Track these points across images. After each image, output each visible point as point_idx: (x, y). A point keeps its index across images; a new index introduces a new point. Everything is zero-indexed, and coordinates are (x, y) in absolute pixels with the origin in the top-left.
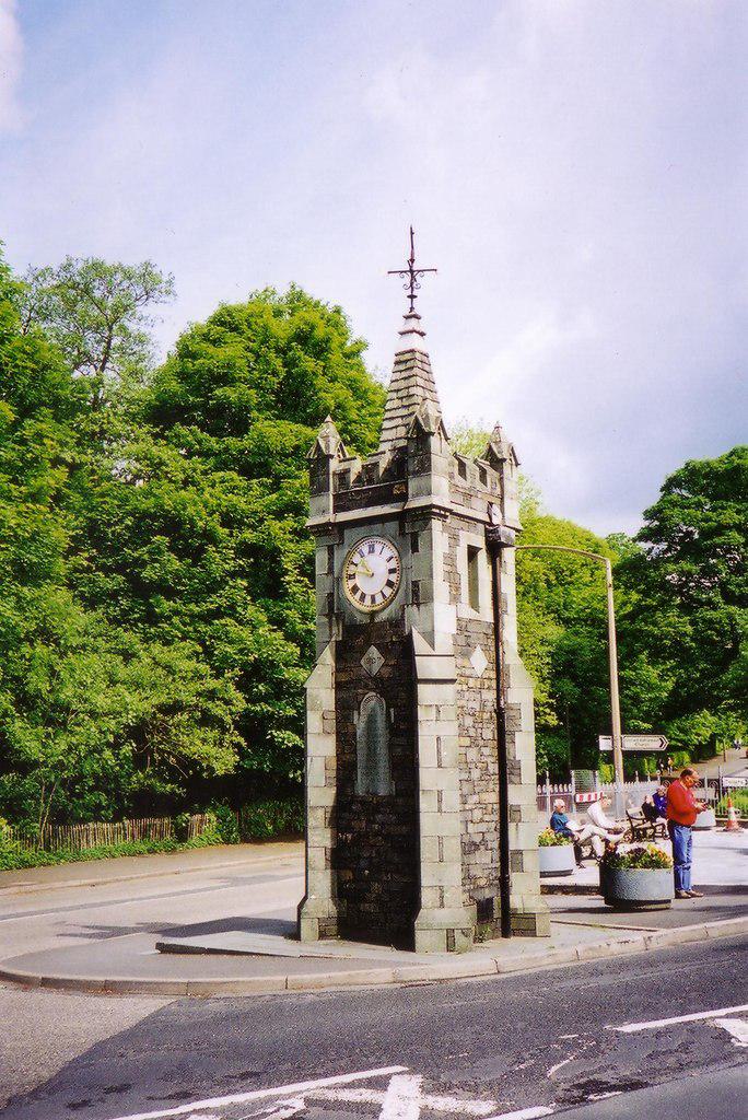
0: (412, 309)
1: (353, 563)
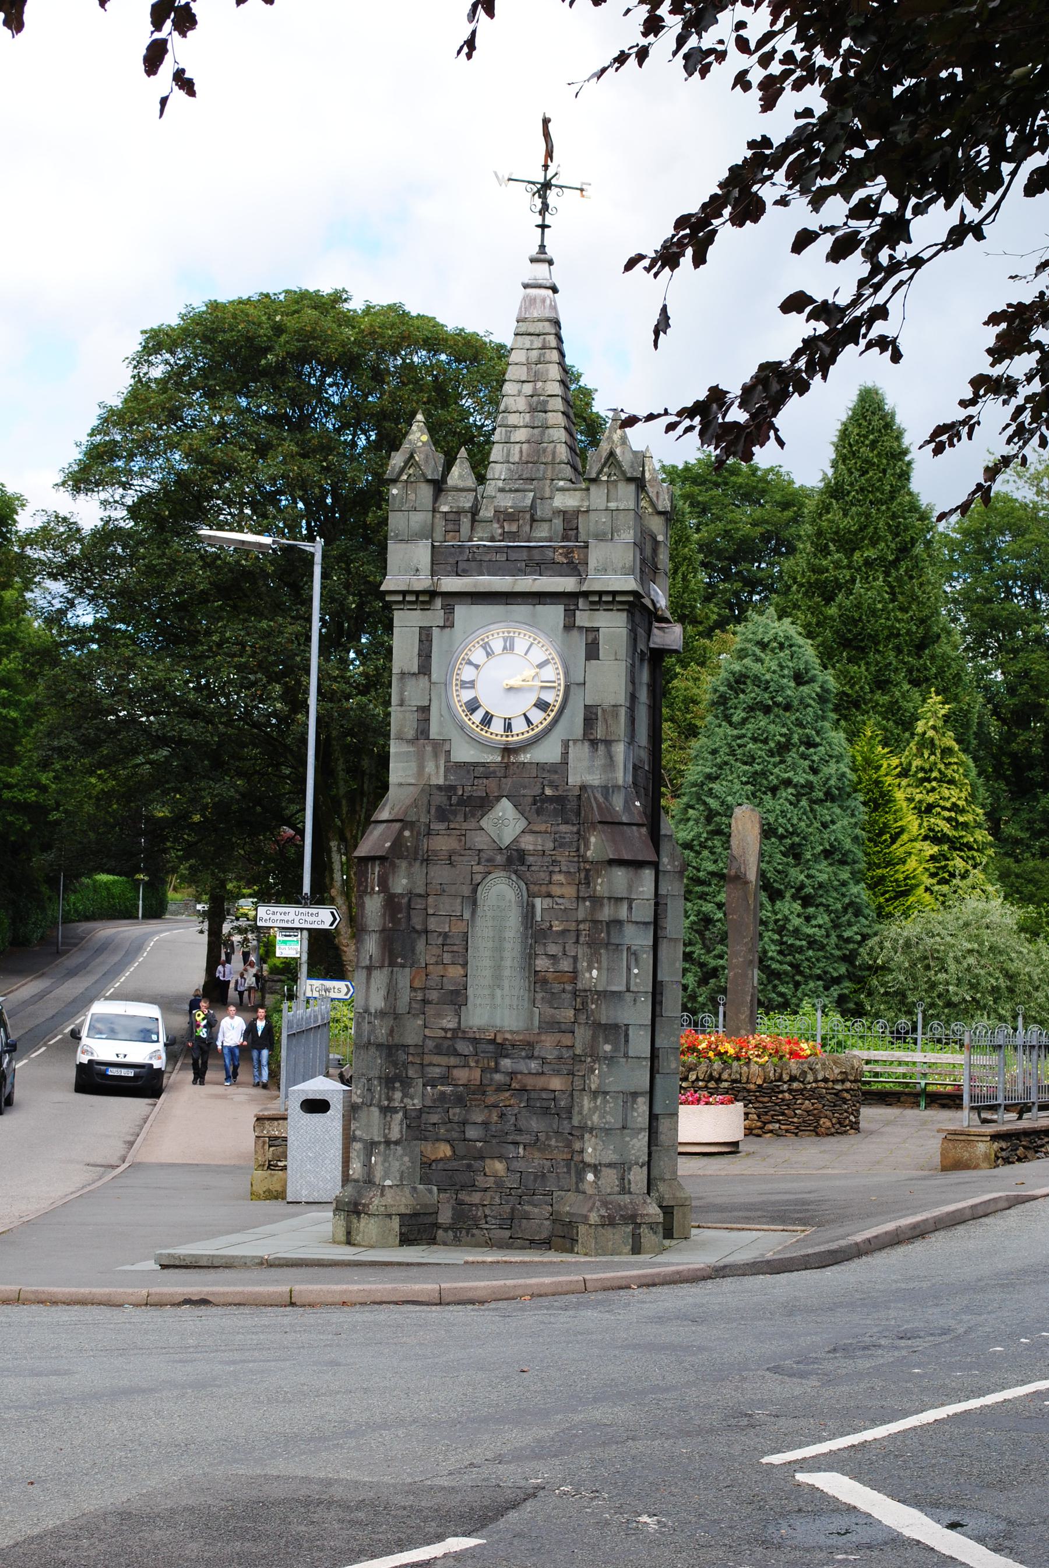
0: (542, 247)
1: (470, 663)
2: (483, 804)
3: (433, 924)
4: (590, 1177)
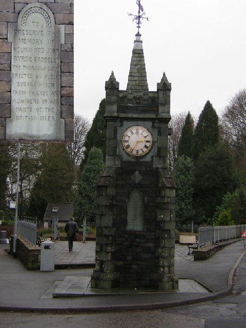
0: (138, 32)
2: (133, 172)
4: (162, 269)
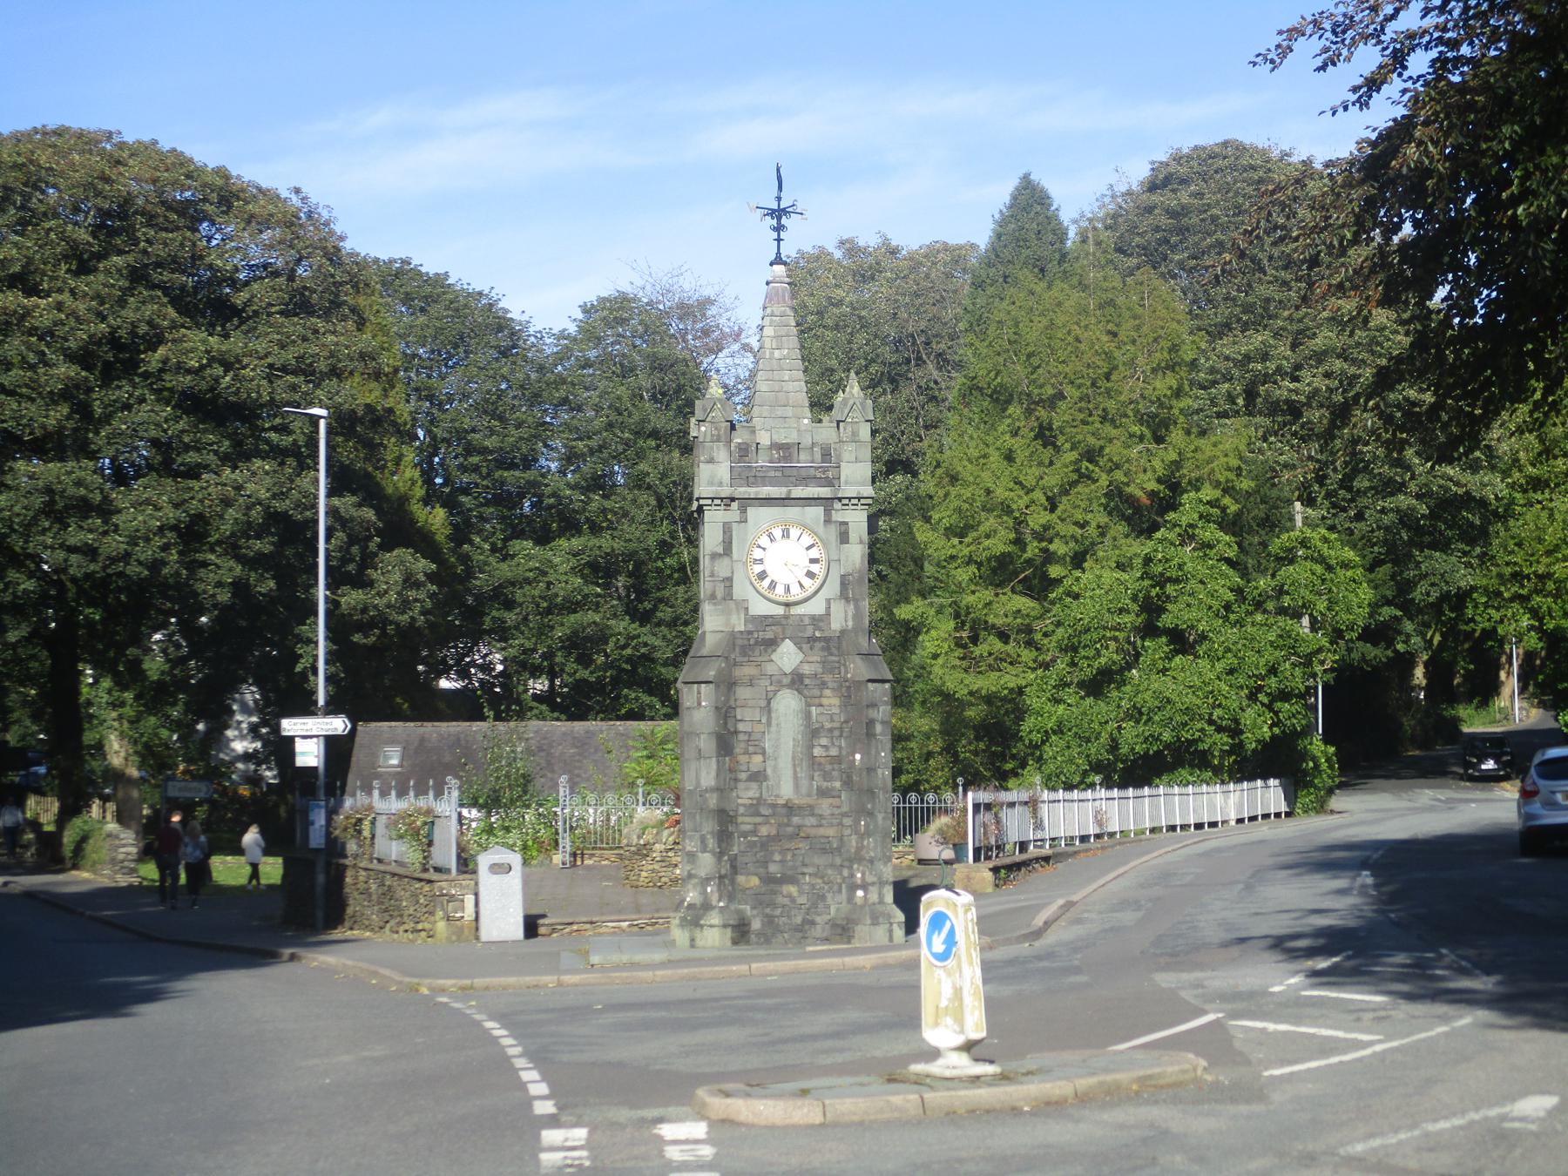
2: (772, 644)
3: (741, 727)
